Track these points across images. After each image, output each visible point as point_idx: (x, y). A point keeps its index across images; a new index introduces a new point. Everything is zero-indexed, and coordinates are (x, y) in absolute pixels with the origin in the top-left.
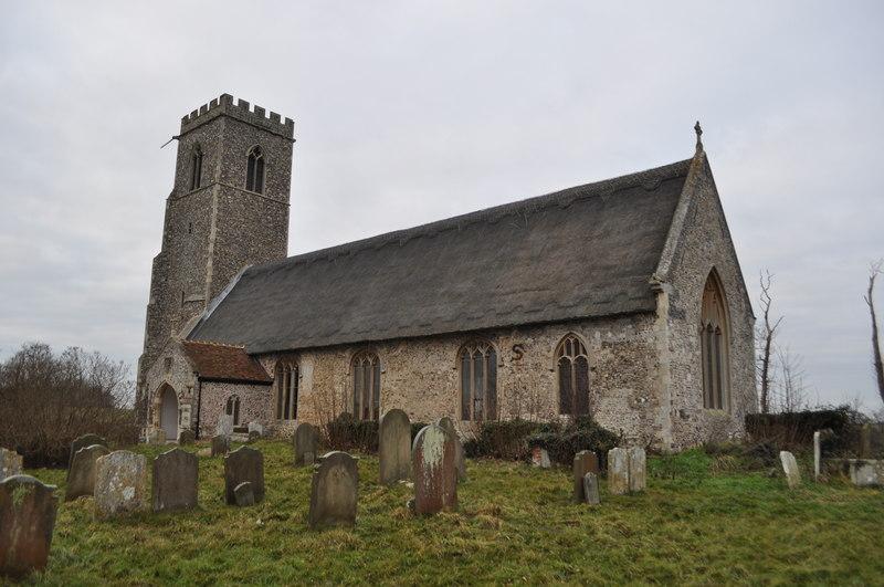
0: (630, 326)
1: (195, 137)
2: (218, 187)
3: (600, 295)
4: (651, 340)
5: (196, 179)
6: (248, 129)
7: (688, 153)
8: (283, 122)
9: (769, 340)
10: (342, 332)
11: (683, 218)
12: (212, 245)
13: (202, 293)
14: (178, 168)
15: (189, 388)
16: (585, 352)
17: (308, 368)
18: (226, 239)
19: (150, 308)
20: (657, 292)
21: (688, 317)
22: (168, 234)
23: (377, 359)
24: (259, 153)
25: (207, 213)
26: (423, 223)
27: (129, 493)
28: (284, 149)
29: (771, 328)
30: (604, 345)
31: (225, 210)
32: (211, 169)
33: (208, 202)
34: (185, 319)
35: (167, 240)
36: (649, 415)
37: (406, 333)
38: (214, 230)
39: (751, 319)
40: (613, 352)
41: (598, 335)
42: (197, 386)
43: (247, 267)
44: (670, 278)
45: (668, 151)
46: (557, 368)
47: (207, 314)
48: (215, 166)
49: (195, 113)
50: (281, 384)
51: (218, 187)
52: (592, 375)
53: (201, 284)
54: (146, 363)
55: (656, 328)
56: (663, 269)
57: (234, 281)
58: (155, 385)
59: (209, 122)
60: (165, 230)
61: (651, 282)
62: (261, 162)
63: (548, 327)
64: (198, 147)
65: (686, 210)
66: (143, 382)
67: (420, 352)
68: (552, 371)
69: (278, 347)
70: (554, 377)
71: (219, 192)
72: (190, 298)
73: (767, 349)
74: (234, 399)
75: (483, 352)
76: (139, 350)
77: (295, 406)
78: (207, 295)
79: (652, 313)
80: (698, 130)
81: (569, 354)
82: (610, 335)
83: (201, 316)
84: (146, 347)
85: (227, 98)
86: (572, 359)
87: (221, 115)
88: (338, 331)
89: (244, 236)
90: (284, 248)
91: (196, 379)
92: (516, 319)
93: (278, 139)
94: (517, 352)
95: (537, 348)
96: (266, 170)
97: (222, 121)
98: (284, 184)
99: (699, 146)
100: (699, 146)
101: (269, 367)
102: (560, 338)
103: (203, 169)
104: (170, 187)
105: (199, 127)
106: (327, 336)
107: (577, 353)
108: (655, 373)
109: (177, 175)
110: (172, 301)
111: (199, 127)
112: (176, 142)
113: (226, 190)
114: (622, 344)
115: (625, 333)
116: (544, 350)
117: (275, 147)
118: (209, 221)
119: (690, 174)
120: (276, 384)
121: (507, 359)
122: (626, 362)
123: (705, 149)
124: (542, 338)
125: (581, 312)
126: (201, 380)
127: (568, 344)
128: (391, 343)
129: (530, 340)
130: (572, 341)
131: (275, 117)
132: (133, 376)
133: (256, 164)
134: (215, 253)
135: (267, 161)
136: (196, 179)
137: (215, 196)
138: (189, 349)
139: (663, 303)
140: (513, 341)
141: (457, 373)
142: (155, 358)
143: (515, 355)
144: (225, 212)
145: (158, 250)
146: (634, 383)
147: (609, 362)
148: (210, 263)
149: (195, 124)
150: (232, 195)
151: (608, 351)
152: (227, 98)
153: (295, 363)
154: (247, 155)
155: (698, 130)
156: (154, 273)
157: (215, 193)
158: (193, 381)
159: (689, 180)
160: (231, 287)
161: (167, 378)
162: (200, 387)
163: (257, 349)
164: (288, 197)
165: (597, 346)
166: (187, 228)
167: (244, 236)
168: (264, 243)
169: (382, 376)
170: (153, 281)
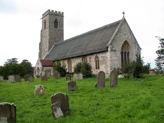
1: (44, 18)
4: (107, 56)
5: (45, 27)
6: (54, 16)
7: (120, 18)
8: (61, 13)
11: (116, 32)
13: (47, 49)
19: (39, 53)
21: (117, 51)
23: (71, 61)
26: (70, 38)
27: (12, 80)
28: (62, 19)
30: (101, 57)
35: (41, 39)
36: (107, 69)
39: (140, 50)
41: (100, 55)
43: (55, 44)
44: (111, 44)
45: (119, 18)
46: (95, 61)
52: (100, 62)
61: (107, 45)
62: (57, 22)
64: (45, 20)
70: (95, 63)
71: (49, 29)
74: (50, 69)
75: (85, 59)
77: (71, 69)
79: (107, 51)
80: (124, 13)
85: (49, 10)
86: (97, 59)
87: (48, 14)
90: (63, 39)
91: (42, 66)
92: (89, 53)
93: (60, 17)
95: (92, 58)
96: (58, 23)
98: (62, 26)
99: (124, 16)
100: (124, 16)
103: (46, 25)
105: (45, 16)
111: (45, 16)
113: (50, 29)
117: (60, 18)
121: (89, 60)
122: (104, 60)
126: (43, 66)
128: (73, 58)
131: (59, 12)
133: (56, 23)
134: (49, 41)
135: (58, 22)
136: (45, 27)
139: (109, 49)
140: (89, 57)
143: (90, 59)
144: (50, 33)
147: (102, 60)
148: (48, 44)
149: (44, 16)
151: (102, 58)
154: (54, 21)
155: (124, 13)
163: (54, 60)
165: (100, 56)
168: (59, 38)
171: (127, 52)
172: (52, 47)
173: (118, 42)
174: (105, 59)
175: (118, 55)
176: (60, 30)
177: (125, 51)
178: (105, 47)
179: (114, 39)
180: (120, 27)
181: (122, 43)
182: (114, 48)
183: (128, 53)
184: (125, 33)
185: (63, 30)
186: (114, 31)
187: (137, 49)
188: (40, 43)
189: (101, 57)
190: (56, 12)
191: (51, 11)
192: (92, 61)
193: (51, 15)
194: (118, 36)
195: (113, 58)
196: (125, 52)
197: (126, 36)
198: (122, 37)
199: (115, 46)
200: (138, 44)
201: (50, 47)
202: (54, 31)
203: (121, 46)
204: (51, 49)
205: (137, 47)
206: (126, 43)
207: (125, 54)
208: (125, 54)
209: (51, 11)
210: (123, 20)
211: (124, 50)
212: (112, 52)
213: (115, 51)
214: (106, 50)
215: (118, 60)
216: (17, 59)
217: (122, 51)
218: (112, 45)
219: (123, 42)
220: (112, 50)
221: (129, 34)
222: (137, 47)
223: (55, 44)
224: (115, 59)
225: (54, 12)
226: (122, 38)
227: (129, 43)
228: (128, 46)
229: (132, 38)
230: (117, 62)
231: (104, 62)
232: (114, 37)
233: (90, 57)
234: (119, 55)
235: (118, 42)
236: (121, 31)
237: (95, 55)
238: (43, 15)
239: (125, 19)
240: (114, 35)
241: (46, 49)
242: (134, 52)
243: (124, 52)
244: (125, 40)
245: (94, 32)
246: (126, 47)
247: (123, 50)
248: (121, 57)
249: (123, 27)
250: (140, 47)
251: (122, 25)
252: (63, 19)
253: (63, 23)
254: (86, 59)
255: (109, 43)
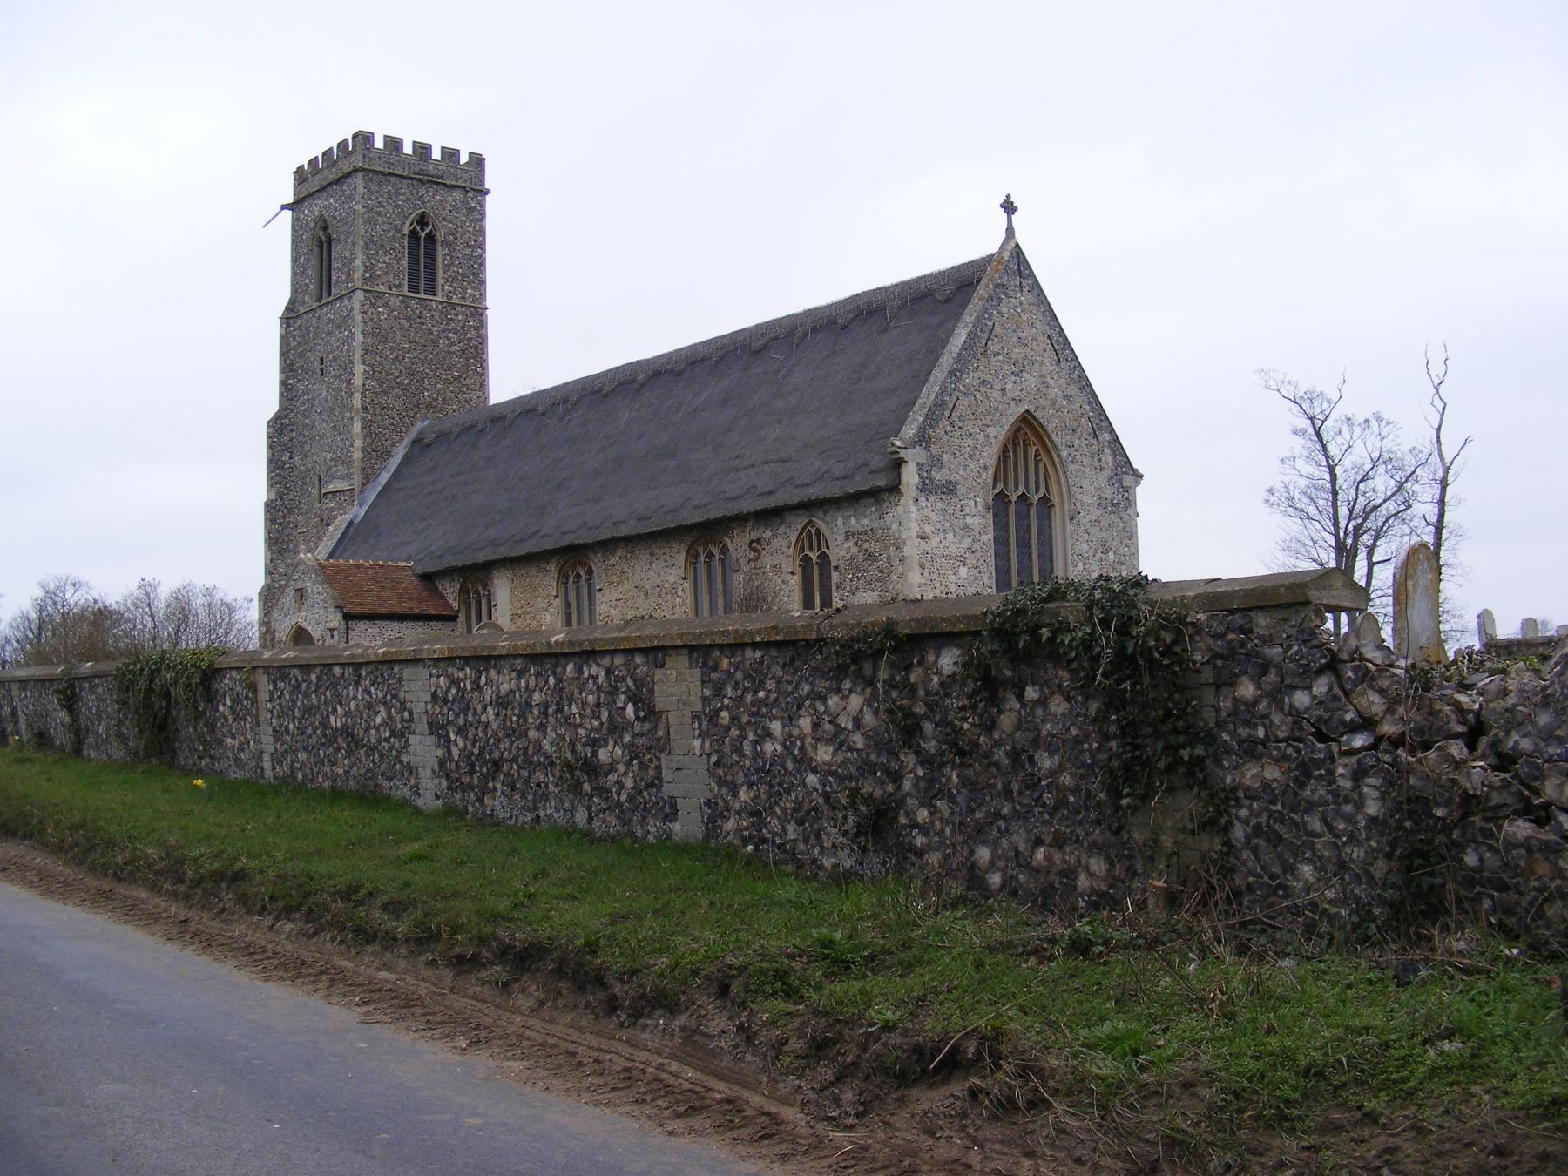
0: (873, 509)
1: (317, 207)
2: (359, 295)
3: (839, 470)
4: (895, 527)
5: (325, 282)
6: (403, 186)
9: (1444, 485)
10: (542, 533)
12: (357, 396)
13: (349, 477)
14: (295, 261)
15: (332, 630)
16: (828, 547)
17: (503, 590)
18: (380, 382)
19: (269, 506)
20: (898, 464)
21: (961, 490)
22: (287, 378)
23: (590, 572)
24: (427, 225)
25: (346, 341)
28: (471, 210)
29: (1448, 460)
31: (376, 333)
32: (348, 264)
33: (344, 322)
34: (325, 522)
35: (286, 388)
37: (623, 531)
38: (359, 369)
39: (1128, 480)
40: (856, 544)
41: (840, 522)
42: (343, 627)
43: (419, 426)
44: (923, 439)
46: (798, 570)
47: (358, 511)
48: (353, 259)
49: (314, 162)
50: (468, 617)
51: (359, 295)
52: (835, 576)
53: (345, 461)
54: (269, 597)
55: (900, 509)
56: (910, 430)
57: (400, 452)
58: (283, 631)
59: (337, 181)
60: (282, 370)
62: (431, 238)
63: (787, 514)
65: (964, 337)
66: (266, 620)
67: (642, 556)
68: (793, 573)
69: (458, 561)
70: (795, 581)
72: (331, 488)
73: (1442, 502)
76: (258, 580)
78: (357, 480)
79: (894, 489)
80: (1009, 207)
81: (811, 549)
82: (853, 521)
83: (348, 517)
84: (269, 573)
86: (814, 556)
87: (356, 170)
88: (538, 531)
89: (411, 373)
90: (483, 386)
91: (339, 617)
92: (748, 505)
93: (458, 194)
94: (755, 550)
95: (776, 543)
96: (441, 252)
97: (358, 180)
98: (474, 273)
99: (1010, 231)
100: (1010, 231)
101: (450, 591)
102: (800, 527)
103: (335, 264)
104: (284, 295)
105: (323, 189)
106: (523, 540)
107: (819, 548)
108: (900, 570)
109: (294, 274)
110: (304, 491)
111: (323, 189)
112: (288, 214)
113: (374, 298)
114: (865, 532)
115: (864, 520)
116: (781, 547)
118: (350, 354)
119: (985, 280)
120: (462, 618)
122: (871, 557)
123: (1020, 237)
124: (782, 529)
125: (816, 492)
126: (348, 617)
127: (809, 534)
129: (768, 533)
130: (813, 531)
131: (450, 154)
132: (253, 614)
134: (365, 409)
135: (440, 236)
136: (325, 282)
137: (356, 311)
138: (326, 572)
139: (910, 476)
140: (751, 533)
141: (687, 585)
142: (282, 588)
144: (374, 335)
145: (272, 406)
146: (879, 584)
147: (854, 558)
148: (357, 426)
149: (315, 183)
150: (385, 305)
151: (850, 544)
152: (363, 138)
153: (486, 585)
154: (406, 231)
155: (1009, 207)
156: (271, 447)
157: (357, 306)
158: (336, 620)
159: (982, 290)
160: (394, 463)
161: (302, 619)
162: (348, 629)
163: (431, 567)
164: (483, 295)
165: (838, 531)
166: (317, 365)
167: (411, 373)
168: (445, 382)
169: (599, 596)
170: (270, 461)
171: (1035, 499)
172: (389, 454)
173: (969, 426)
174: (874, 547)
175: (969, 520)
176: (453, 306)
177: (1042, 491)
178: (877, 462)
179: (939, 404)
180: (985, 310)
181: (1000, 431)
182: (945, 471)
183: (1045, 501)
184: (1018, 353)
185: (478, 312)
186: (944, 342)
187: (1106, 473)
188: (277, 417)
189: (841, 538)
190: (423, 150)
191: (379, 143)
192: (777, 569)
193: (377, 178)
194: (969, 379)
195: (935, 541)
196: (1023, 498)
197: (1031, 381)
198: (997, 386)
199: (945, 457)
200: (1117, 440)
201: (376, 453)
202: (408, 319)
203: (990, 455)
204: (385, 477)
205: (1110, 459)
206: (1028, 431)
207: (1023, 517)
208: (1023, 517)
209: (379, 143)
210: (1006, 255)
211: (1011, 485)
212: (932, 498)
213: (949, 489)
214: (881, 482)
215: (971, 560)
216: (1279, 526)
217: (997, 491)
218: (927, 448)
219: (1007, 428)
220: (926, 487)
221: (1049, 367)
222: (1108, 458)
223: (419, 426)
224: (952, 550)
225: (408, 149)
226: (996, 395)
227: (1050, 428)
228: (1044, 457)
229: (1073, 390)
230: (963, 571)
231: (873, 572)
232: (943, 390)
233: (755, 535)
234: (979, 518)
235: (969, 426)
236: (994, 346)
237: (798, 522)
238: (300, 176)
239: (1018, 253)
240: (939, 374)
241: (342, 470)
242: (1087, 499)
243: (1014, 498)
244: (1022, 410)
245: (776, 338)
246: (1026, 458)
247: (1005, 484)
248: (991, 536)
249: (1004, 310)
250: (1128, 462)
251: (1000, 300)
252: (478, 214)
253: (482, 247)
254: (725, 550)
255: (910, 430)
